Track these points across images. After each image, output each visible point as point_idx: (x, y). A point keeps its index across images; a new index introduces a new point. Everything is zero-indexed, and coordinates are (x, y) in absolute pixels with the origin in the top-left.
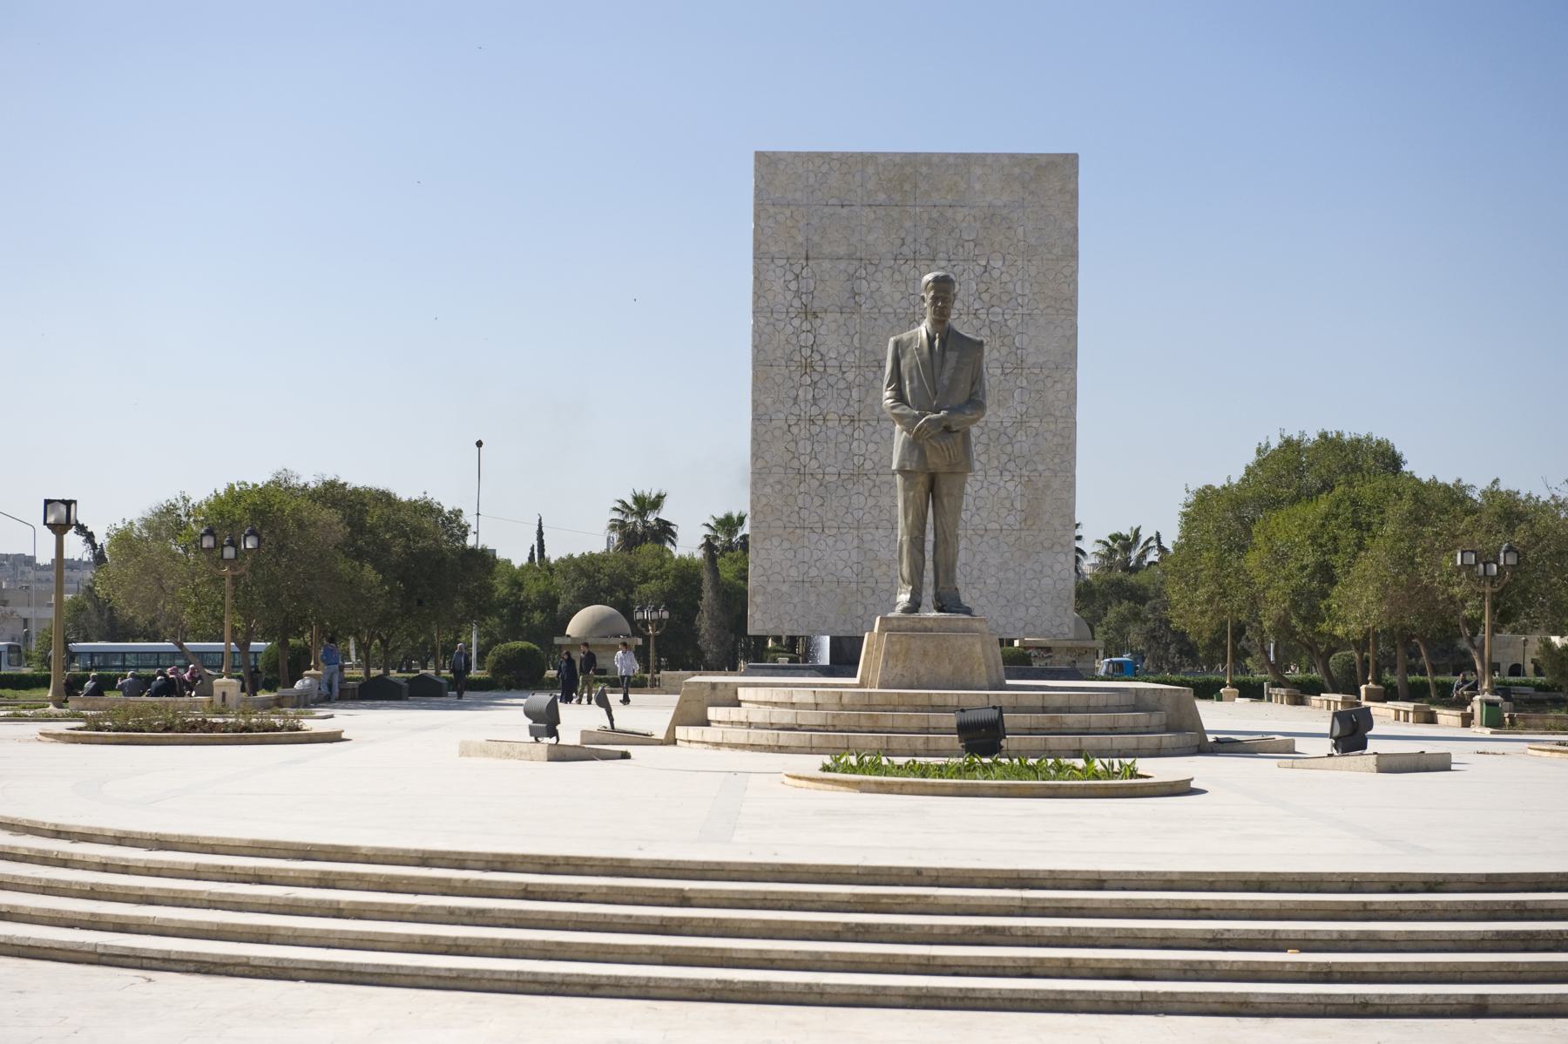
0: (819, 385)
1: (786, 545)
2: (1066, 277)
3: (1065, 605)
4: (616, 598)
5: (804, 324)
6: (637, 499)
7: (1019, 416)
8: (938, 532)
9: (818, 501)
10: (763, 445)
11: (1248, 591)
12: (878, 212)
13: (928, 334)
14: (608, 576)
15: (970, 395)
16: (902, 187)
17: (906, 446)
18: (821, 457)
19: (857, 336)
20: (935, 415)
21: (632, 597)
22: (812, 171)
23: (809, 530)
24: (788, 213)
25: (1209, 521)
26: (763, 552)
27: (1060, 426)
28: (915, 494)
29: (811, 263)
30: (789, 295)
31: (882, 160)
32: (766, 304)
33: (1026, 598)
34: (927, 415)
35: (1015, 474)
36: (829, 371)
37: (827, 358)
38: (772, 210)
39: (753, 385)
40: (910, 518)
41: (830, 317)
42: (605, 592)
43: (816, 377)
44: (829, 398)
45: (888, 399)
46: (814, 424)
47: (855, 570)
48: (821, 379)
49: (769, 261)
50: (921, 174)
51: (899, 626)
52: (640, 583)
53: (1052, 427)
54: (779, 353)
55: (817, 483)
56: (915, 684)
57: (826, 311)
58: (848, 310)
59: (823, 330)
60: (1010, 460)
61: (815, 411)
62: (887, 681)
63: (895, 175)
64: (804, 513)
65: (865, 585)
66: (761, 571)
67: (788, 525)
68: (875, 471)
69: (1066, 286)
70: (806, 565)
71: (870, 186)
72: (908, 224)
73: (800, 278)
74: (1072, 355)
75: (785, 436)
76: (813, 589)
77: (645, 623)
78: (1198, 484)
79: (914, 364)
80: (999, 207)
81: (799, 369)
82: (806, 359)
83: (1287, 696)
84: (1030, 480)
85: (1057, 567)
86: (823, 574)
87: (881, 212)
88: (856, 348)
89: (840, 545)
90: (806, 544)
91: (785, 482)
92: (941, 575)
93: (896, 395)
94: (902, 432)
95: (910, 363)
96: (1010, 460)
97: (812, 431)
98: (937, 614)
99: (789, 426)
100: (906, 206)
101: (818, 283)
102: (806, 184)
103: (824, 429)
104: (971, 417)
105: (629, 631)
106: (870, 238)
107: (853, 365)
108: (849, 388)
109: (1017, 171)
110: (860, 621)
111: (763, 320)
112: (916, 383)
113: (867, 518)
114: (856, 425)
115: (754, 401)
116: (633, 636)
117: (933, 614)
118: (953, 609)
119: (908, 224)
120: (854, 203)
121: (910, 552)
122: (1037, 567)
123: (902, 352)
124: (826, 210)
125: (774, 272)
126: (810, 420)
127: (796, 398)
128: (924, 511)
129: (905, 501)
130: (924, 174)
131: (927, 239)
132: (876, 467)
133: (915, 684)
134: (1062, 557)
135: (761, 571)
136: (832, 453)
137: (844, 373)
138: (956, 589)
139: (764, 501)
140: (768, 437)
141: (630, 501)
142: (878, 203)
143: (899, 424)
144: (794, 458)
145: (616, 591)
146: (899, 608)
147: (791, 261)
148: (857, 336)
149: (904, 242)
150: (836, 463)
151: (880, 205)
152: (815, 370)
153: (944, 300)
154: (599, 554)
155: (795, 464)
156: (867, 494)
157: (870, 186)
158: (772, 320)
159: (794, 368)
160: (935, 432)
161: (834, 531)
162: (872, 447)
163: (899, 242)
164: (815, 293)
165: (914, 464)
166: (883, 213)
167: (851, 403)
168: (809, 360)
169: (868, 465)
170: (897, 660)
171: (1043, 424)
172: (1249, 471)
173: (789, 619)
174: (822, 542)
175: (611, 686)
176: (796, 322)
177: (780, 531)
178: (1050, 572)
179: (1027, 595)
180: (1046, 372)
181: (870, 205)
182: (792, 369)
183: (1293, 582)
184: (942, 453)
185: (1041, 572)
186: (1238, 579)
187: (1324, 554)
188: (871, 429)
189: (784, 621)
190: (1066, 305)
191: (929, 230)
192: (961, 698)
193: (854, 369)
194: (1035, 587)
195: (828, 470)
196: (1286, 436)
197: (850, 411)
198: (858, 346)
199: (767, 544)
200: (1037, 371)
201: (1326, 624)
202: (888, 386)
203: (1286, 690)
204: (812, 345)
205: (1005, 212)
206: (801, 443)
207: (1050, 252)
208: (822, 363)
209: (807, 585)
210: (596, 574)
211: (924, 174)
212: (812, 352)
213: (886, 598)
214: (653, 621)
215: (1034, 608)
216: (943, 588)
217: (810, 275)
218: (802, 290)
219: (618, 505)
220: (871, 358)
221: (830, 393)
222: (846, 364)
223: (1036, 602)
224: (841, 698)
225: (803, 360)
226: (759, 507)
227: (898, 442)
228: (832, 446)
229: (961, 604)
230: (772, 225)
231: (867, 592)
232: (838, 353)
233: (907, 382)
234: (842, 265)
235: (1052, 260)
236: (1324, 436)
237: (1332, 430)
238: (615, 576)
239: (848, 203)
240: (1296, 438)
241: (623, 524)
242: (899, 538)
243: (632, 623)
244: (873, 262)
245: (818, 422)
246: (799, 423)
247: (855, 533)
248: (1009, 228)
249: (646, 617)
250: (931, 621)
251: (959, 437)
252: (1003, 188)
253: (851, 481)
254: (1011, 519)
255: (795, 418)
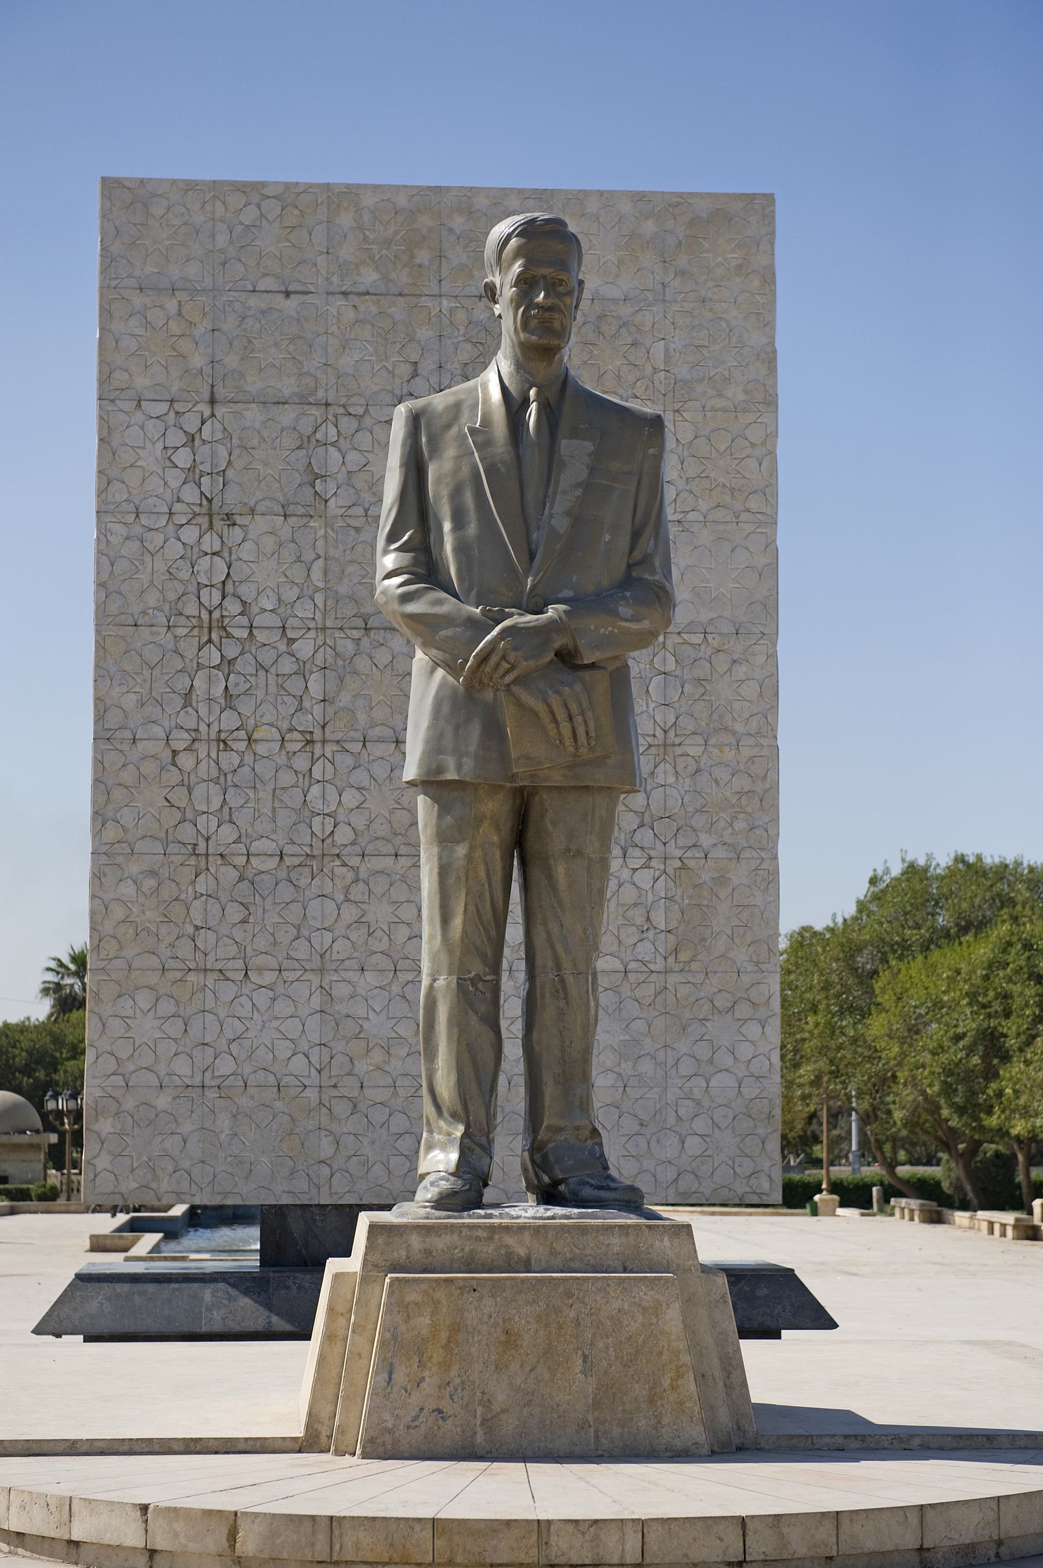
0: (239, 666)
1: (167, 1007)
2: (753, 445)
3: (761, 1131)
4: (36, 1079)
5: (207, 537)
6: (74, 959)
7: (659, 733)
8: (539, 961)
9: (235, 913)
10: (118, 794)
11: (871, 1068)
12: (362, 308)
13: (504, 389)
14: (27, 1052)
15: (629, 566)
16: (412, 256)
17: (446, 709)
18: (243, 819)
19: (320, 563)
20: (530, 617)
21: (56, 1077)
22: (222, 221)
23: (216, 975)
24: (172, 306)
25: (813, 974)
26: (115, 1024)
27: (746, 753)
28: (472, 848)
29: (220, 410)
30: (175, 479)
31: (369, 201)
32: (125, 497)
33: (679, 1118)
34: (511, 615)
35: (653, 853)
36: (260, 636)
37: (255, 610)
38: (138, 300)
39: (97, 666)
40: (457, 922)
41: (260, 524)
42: (21, 1072)
43: (231, 650)
44: (260, 694)
45: (389, 575)
46: (227, 748)
47: (315, 1059)
48: (242, 653)
49: (129, 406)
50: (451, 230)
51: (428, 1252)
52: (68, 1059)
53: (730, 754)
54: (152, 599)
55: (234, 875)
56: (480, 1438)
57: (252, 512)
58: (301, 510)
59: (247, 552)
60: (641, 825)
61: (229, 721)
62: (390, 1431)
63: (397, 233)
64: (207, 939)
65: (336, 1093)
66: (111, 1065)
67: (171, 964)
68: (358, 849)
69: (752, 463)
70: (209, 1051)
71: (347, 252)
72: (424, 334)
73: (197, 442)
74: (769, 606)
75: (165, 775)
76: (222, 1103)
77: (59, 1114)
78: (805, 923)
79: (466, 470)
80: (614, 300)
81: (196, 632)
82: (210, 612)
83: (920, 1210)
84: (684, 867)
85: (745, 1051)
86: (247, 1070)
87: (369, 307)
88: (317, 590)
89: (283, 1007)
90: (210, 1004)
91: (165, 873)
92: (550, 1090)
93: (415, 562)
94: (432, 671)
95: (456, 471)
96: (641, 825)
97: (224, 765)
98: (541, 1210)
99: (175, 753)
100: (420, 296)
101: (236, 452)
102: (210, 247)
103: (249, 759)
104: (634, 626)
105: (39, 1125)
106: (347, 362)
107: (312, 625)
108: (302, 673)
109: (649, 227)
110: (326, 1171)
111: (118, 528)
112: (472, 529)
113: (342, 948)
114: (318, 749)
115: (98, 700)
116: (45, 1131)
117: (531, 1212)
118: (587, 1192)
119: (424, 334)
120: (312, 288)
121: (457, 1021)
122: (703, 1051)
123: (430, 441)
124: (253, 301)
125: (142, 428)
126: (218, 740)
127: (188, 695)
128: (500, 903)
129: (443, 872)
130: (458, 232)
131: (466, 364)
132: (360, 840)
133: (480, 1438)
134: (753, 1030)
135: (111, 1065)
136: (267, 810)
137: (293, 641)
138: (595, 1132)
139: (119, 912)
140: (128, 776)
141: (66, 960)
142: (362, 289)
143: (425, 645)
144: (183, 820)
145: (34, 1070)
146: (426, 1193)
147: (178, 407)
148: (320, 563)
149: (415, 370)
150: (274, 832)
151: (368, 293)
152: (229, 636)
153: (552, 287)
154: (17, 1025)
155: (187, 833)
156: (342, 897)
157: (347, 252)
158: (138, 530)
159: (185, 631)
160: (532, 664)
161: (269, 977)
162: (350, 798)
163: (405, 370)
164: (230, 473)
165: (469, 763)
166: (374, 309)
167: (307, 704)
168: (216, 614)
169: (343, 835)
170: (421, 1364)
171: (710, 749)
172: (862, 907)
173: (171, 1169)
174: (244, 999)
175: (12, 1200)
176: (190, 534)
177: (153, 979)
178: (729, 1061)
179: (682, 1112)
180: (714, 641)
181: (345, 294)
182: (181, 632)
183: (944, 1058)
184: (551, 727)
185: (711, 1061)
186: (855, 1052)
187: (989, 1016)
188: (349, 760)
189: (159, 1172)
190: (754, 504)
191: (468, 347)
192: (650, 1537)
193: (312, 634)
194: (697, 1093)
195: (257, 846)
196: (909, 858)
197: (305, 722)
198: (321, 585)
199: (125, 1006)
200: (696, 639)
201: (996, 1116)
202: (392, 538)
203: (919, 1202)
204: (224, 583)
205: (626, 311)
206: (199, 791)
207: (720, 395)
208: (244, 621)
209: (212, 1094)
210: (10, 1049)
211: (458, 232)
212: (223, 598)
213: (382, 1120)
214: (69, 1112)
215: (697, 1139)
216: (558, 1130)
217: (219, 436)
218: (202, 468)
219: (53, 965)
220: (349, 610)
221: (262, 685)
222: (296, 622)
223: (700, 1125)
224: (232, 1535)
225: (205, 616)
226: (108, 927)
227: (423, 696)
228: (265, 794)
229: (609, 1177)
230: (138, 332)
231: (341, 1108)
232: (280, 600)
233: (447, 526)
234: (287, 416)
235: (725, 410)
236: (960, 859)
237: (971, 853)
238: (35, 1052)
239: (301, 288)
240: (922, 862)
241: (58, 987)
242: (425, 981)
243: (44, 1116)
244: (351, 410)
245: (235, 746)
246: (196, 745)
247: (316, 981)
248: (634, 344)
249: (60, 1107)
250: (527, 1237)
251: (600, 681)
252: (621, 262)
253: (307, 870)
254: (645, 950)
255: (186, 735)
